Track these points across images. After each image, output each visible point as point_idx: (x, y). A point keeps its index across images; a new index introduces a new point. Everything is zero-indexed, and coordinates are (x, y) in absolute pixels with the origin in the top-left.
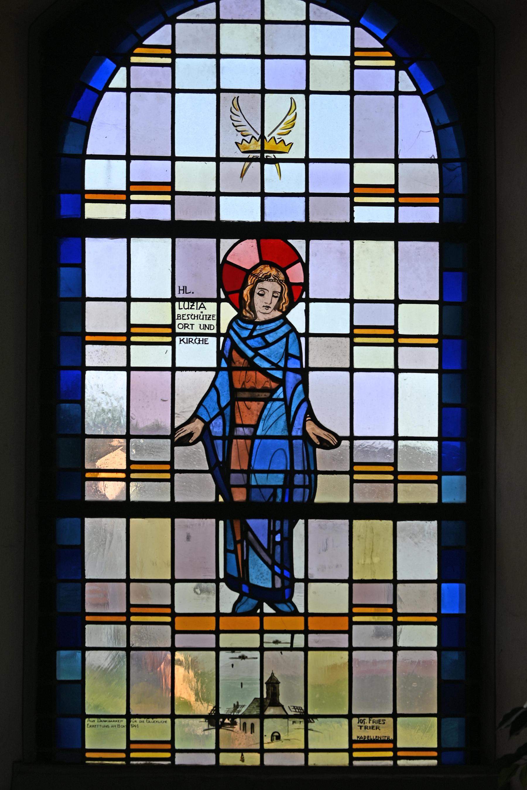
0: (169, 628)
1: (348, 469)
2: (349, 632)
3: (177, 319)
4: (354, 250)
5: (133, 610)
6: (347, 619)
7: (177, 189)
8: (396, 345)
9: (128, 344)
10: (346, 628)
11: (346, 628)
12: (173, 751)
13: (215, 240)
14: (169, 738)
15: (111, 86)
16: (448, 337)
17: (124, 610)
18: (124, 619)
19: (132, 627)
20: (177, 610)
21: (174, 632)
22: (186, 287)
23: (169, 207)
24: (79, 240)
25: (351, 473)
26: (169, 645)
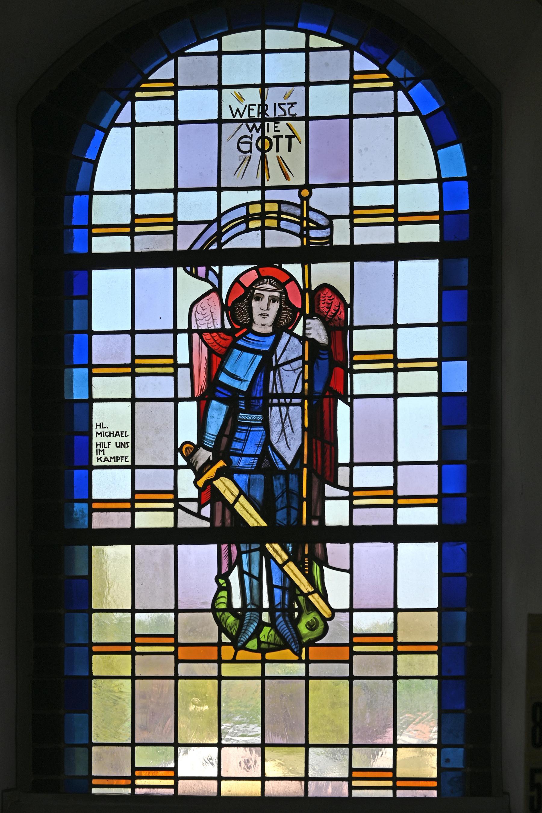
0: (172, 657)
1: (347, 78)
2: (350, 662)
4: (354, 160)
5: (138, 640)
6: (348, 648)
7: (180, 774)
8: (396, 371)
9: (134, 375)
10: (347, 658)
11: (347, 658)
12: (177, 778)
13: (216, 546)
14: (172, 632)
15: (117, 122)
16: (449, 644)
21: (177, 661)
22: (102, 423)
23: (171, 236)
24: (86, 272)
25: (351, 82)
26: (172, 674)
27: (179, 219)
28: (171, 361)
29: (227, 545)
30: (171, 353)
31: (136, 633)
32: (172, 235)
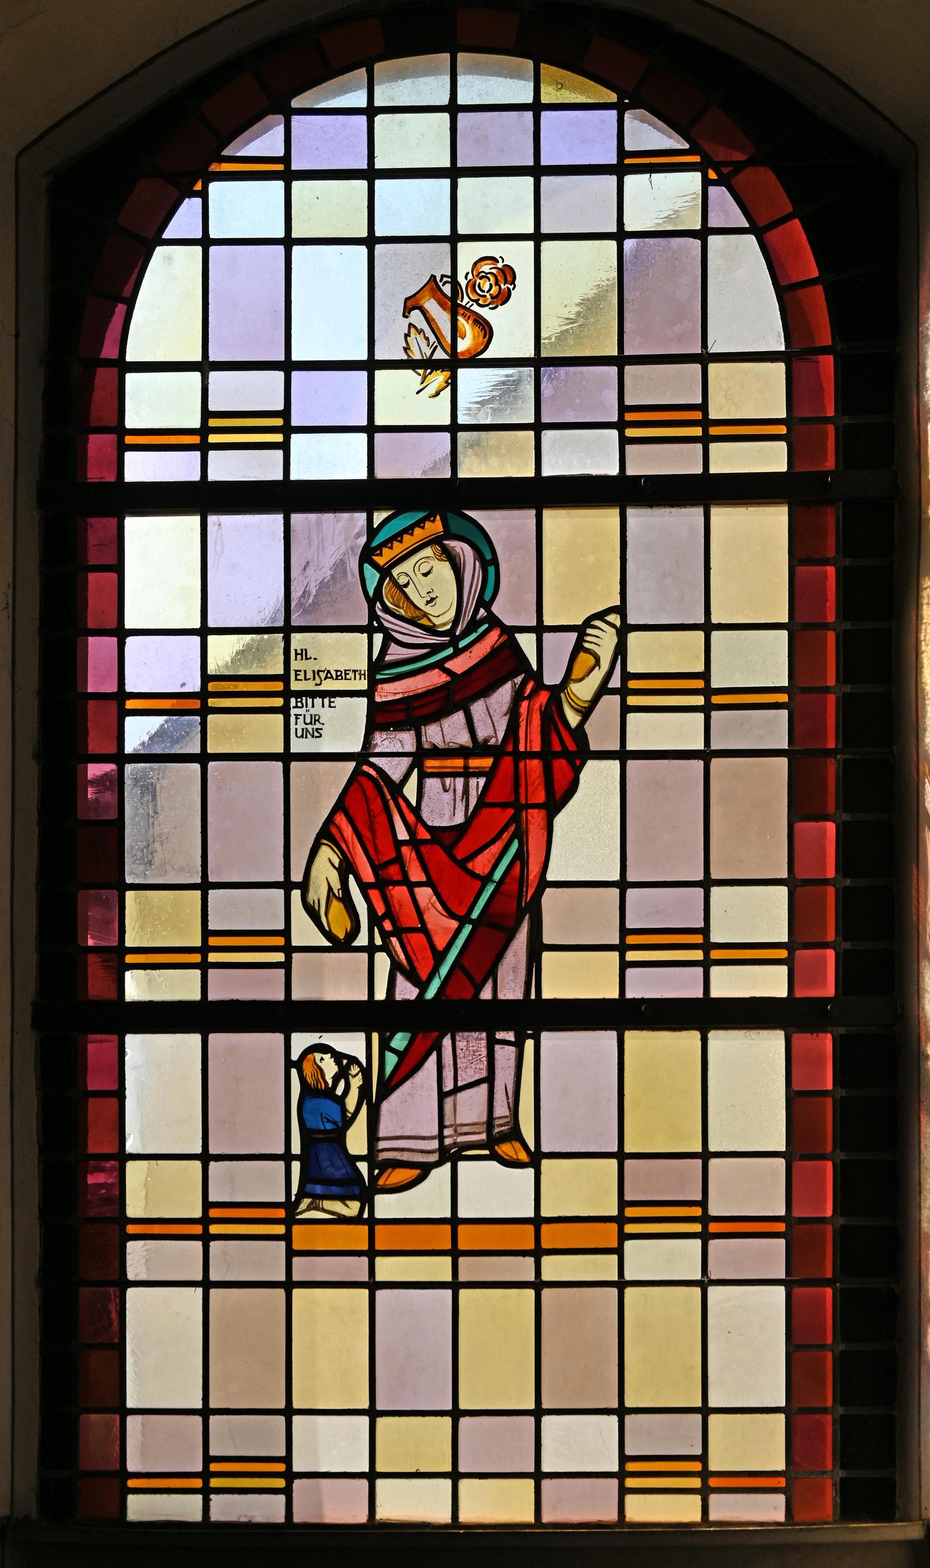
2: (619, 1251)
3: (294, 707)
7: (296, 1468)
8: (705, 1237)
9: (206, 1239)
11: (615, 1245)
17: (199, 1468)
18: (197, 958)
19: (214, 1245)
20: (298, 1466)
21: (291, 1254)
22: (306, 650)
27: (294, 423)
28: (281, 1467)
29: (374, 557)
30: (281, 926)
31: (210, 891)
32: (283, 971)
